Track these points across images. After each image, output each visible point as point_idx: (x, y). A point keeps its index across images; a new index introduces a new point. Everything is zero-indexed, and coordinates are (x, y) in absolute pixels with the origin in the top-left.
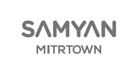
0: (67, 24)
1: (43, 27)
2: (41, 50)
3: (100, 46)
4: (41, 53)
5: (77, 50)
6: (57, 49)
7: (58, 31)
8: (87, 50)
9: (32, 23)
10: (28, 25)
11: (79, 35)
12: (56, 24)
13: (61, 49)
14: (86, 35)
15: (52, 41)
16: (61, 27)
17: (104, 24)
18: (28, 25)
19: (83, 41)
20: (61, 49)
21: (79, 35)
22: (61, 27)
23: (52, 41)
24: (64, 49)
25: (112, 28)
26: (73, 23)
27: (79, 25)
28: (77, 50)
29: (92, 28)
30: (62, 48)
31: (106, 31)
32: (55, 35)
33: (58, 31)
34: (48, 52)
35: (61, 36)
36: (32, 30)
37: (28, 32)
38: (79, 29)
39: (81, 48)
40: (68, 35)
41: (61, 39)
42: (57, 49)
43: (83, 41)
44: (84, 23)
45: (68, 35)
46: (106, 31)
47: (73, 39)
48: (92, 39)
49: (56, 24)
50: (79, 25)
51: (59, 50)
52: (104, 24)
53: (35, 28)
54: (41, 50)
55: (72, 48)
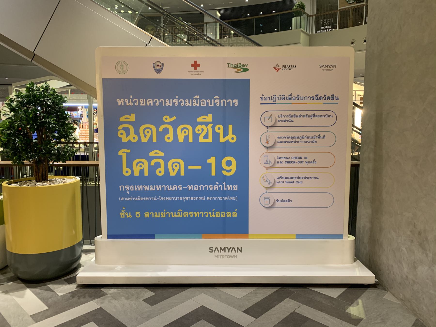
0: (225, 248)
1: (216, 249)
2: (216, 257)
3: (241, 248)
4: (216, 258)
5: (329, 70)
6: (222, 257)
7: (221, 250)
8: (331, 70)
9: (212, 248)
10: (211, 248)
11: (329, 67)
12: (221, 248)
13: (326, 70)
14: (331, 67)
15: (325, 68)
16: (223, 249)
17: (334, 65)
18: (211, 248)
19: (330, 68)
20: (326, 70)
21: (329, 67)
22: (223, 249)
23: (325, 68)
24: (224, 256)
25: (238, 250)
26: (227, 248)
27: (229, 248)
28: (228, 257)
29: (233, 249)
30: (223, 256)
31: (334, 67)
32: (221, 252)
33: (221, 250)
34: (219, 258)
35: (223, 252)
36: (321, 67)
37: (211, 251)
38: (329, 66)
39: (230, 256)
40: (225, 252)
41: (326, 68)
42: (222, 257)
43: (330, 68)
44: (231, 248)
45: (225, 252)
46: (334, 67)
47: (328, 68)
48: (332, 68)
49: (221, 248)
50: (229, 248)
51: (223, 257)
52: (334, 65)
53: (322, 66)
54: (216, 257)
55: (227, 257)
